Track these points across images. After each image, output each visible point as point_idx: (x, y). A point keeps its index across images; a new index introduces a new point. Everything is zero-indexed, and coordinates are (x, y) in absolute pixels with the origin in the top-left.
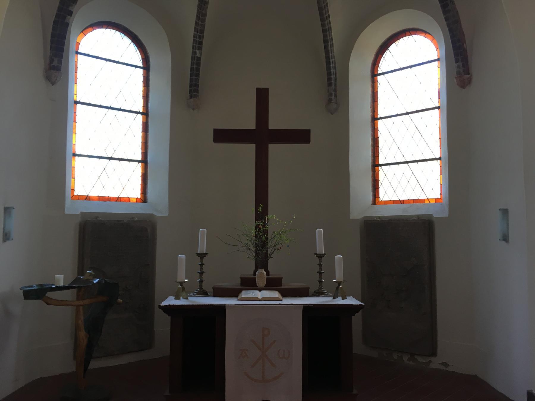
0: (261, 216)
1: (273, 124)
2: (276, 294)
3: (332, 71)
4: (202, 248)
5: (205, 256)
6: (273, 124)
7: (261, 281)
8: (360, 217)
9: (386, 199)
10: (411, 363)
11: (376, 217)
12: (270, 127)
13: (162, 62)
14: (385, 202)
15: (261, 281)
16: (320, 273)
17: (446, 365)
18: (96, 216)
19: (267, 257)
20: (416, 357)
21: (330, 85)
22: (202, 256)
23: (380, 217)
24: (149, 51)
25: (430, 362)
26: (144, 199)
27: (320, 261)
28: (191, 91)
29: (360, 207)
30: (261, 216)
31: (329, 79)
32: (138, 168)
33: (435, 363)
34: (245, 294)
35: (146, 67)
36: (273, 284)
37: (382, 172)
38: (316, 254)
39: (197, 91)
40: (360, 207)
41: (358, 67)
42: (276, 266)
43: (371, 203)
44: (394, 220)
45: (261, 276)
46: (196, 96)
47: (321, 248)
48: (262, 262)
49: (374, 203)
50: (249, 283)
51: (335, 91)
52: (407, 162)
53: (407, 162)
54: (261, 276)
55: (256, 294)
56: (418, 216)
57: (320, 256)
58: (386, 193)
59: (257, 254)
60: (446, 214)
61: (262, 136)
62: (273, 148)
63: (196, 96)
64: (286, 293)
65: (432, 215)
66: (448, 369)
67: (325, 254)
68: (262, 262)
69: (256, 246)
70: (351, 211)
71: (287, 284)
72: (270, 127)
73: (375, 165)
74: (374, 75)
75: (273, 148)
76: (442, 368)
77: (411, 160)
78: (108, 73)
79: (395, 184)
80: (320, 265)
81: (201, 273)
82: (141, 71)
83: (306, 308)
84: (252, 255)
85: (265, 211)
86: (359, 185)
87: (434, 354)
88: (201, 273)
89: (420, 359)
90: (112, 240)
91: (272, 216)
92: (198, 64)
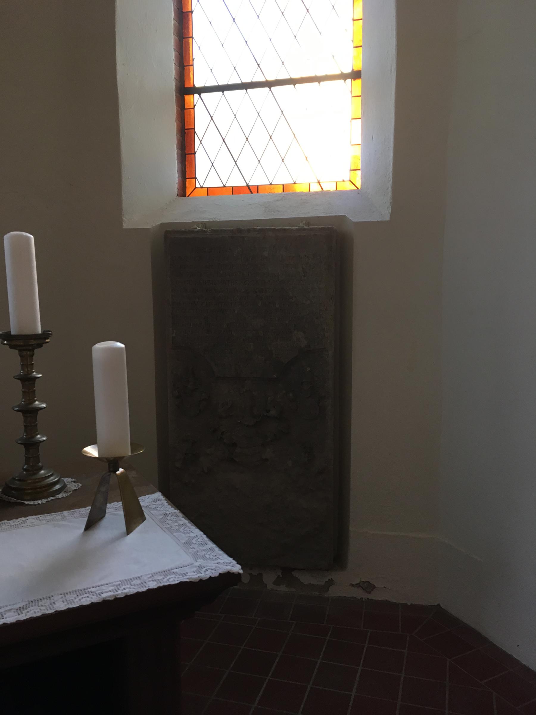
5: (40, 346)
9: (213, 182)
10: (283, 588)
11: (197, 223)
16: (29, 413)
17: (368, 587)
20: (295, 574)
23: (204, 224)
25: (331, 582)
27: (27, 363)
29: (147, 201)
33: (343, 585)
37: (202, 108)
38: (8, 336)
40: (147, 201)
43: (176, 191)
44: (249, 231)
47: (27, 313)
49: (183, 192)
52: (269, 84)
53: (269, 84)
56: (308, 221)
57: (27, 345)
58: (212, 169)
60: (383, 212)
65: (342, 219)
66: (376, 596)
67: (45, 335)
70: (125, 205)
73: (185, 90)
76: (359, 594)
77: (280, 77)
79: (235, 141)
80: (27, 381)
86: (145, 138)
87: (338, 559)
89: (306, 579)
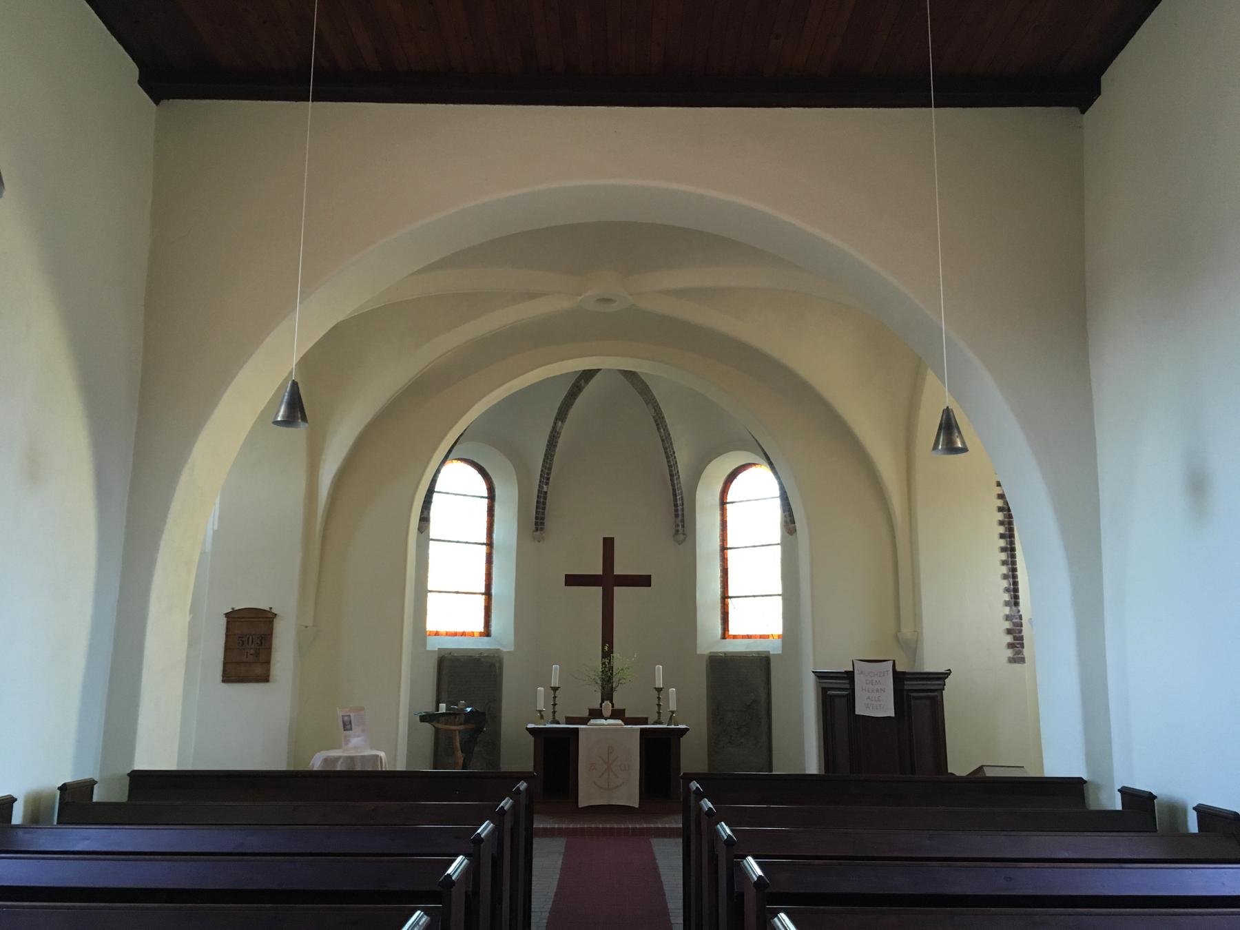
0: (607, 654)
1: (618, 570)
2: (620, 722)
3: (679, 502)
4: (555, 682)
6: (618, 570)
7: (607, 712)
8: (706, 652)
12: (616, 573)
13: (508, 495)
14: (735, 637)
15: (607, 712)
18: (450, 651)
19: (612, 690)
21: (677, 516)
22: (555, 689)
24: (495, 482)
26: (487, 633)
28: (536, 524)
30: (607, 654)
31: (676, 511)
32: (481, 600)
34: (592, 721)
35: (491, 497)
36: (617, 714)
39: (543, 524)
40: (709, 640)
41: (706, 497)
42: (619, 701)
45: (607, 708)
46: (542, 529)
47: (660, 684)
48: (607, 695)
50: (596, 713)
51: (683, 521)
54: (607, 708)
55: (603, 721)
56: (758, 653)
57: (659, 690)
59: (603, 688)
61: (608, 581)
62: (618, 591)
63: (542, 529)
64: (628, 721)
68: (607, 695)
69: (603, 680)
71: (627, 715)
72: (616, 573)
74: (723, 503)
75: (618, 591)
78: (461, 510)
81: (554, 705)
82: (486, 501)
83: (642, 730)
84: (599, 689)
85: (611, 650)
86: (708, 620)
88: (554, 705)
90: (466, 677)
91: (616, 654)
92: (545, 498)
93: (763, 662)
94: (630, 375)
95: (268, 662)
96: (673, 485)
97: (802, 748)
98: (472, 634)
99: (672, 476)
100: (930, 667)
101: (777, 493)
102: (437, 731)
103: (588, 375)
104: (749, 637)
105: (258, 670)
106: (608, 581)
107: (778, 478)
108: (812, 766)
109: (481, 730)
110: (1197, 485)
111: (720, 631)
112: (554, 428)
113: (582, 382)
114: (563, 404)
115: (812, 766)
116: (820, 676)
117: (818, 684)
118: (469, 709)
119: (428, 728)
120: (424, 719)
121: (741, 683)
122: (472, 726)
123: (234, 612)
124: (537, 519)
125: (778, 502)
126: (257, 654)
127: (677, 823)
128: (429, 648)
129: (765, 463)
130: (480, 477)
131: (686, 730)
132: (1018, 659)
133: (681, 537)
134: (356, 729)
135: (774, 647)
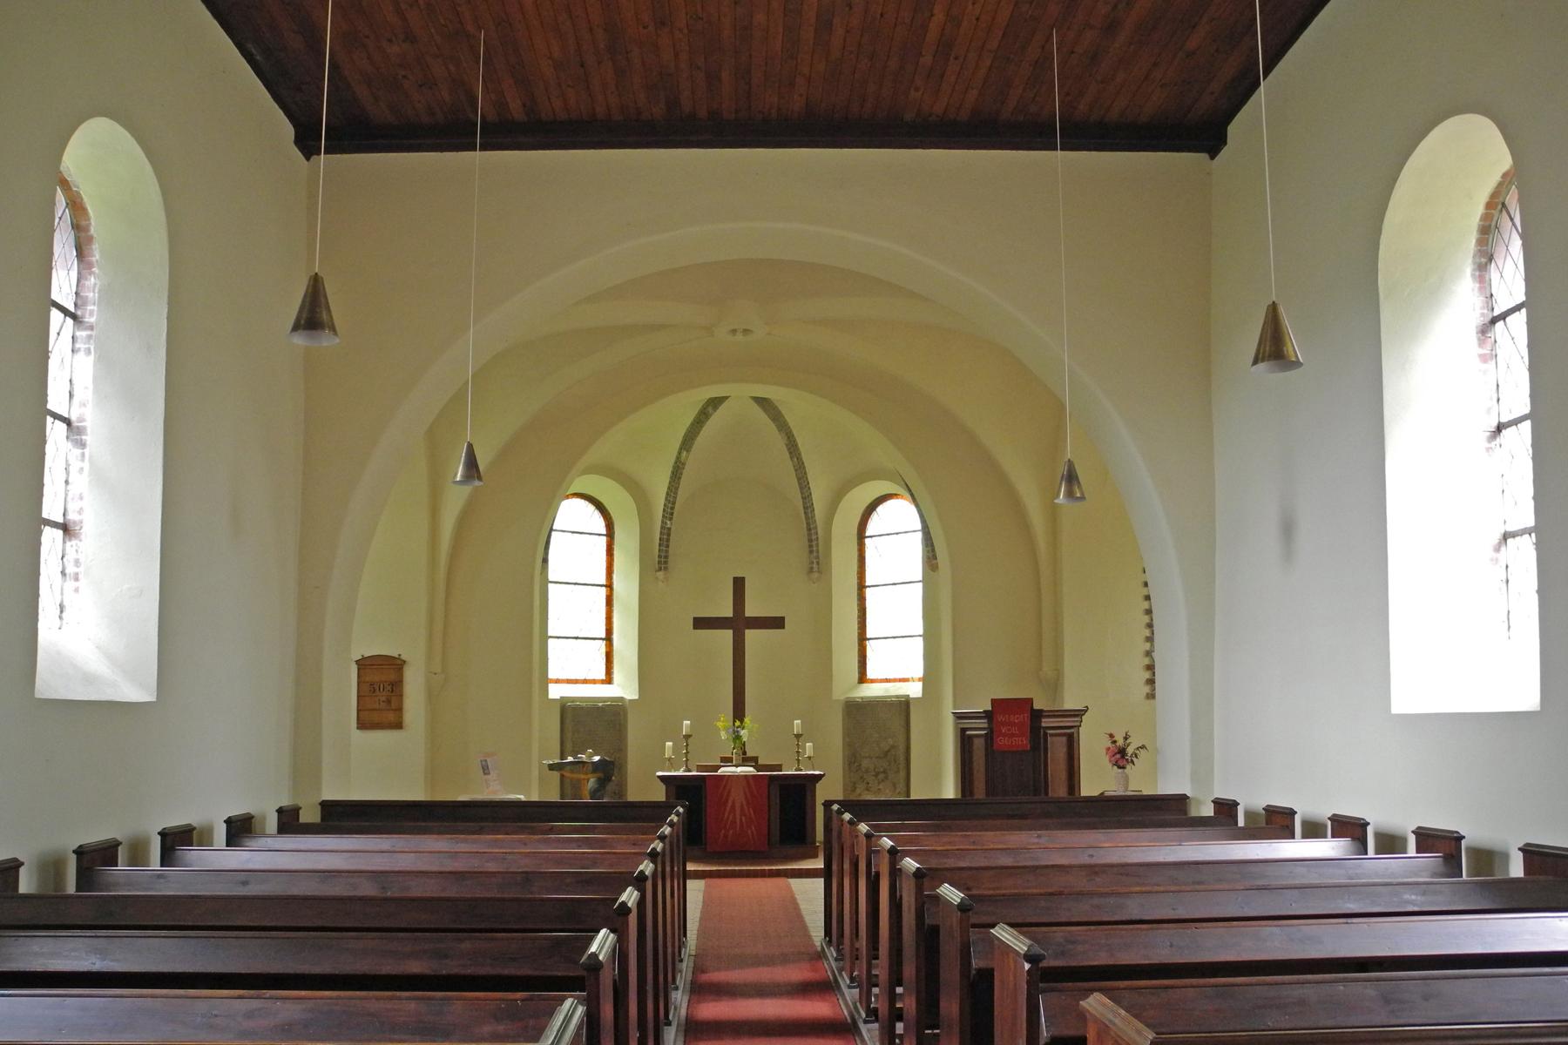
12: (747, 614)
14: (873, 681)
18: (573, 699)
35: (610, 534)
40: (845, 687)
50: (727, 761)
61: (739, 623)
72: (747, 614)
82: (604, 539)
93: (904, 705)
94: (761, 402)
95: (400, 709)
96: (807, 518)
97: (939, 778)
98: (594, 682)
99: (805, 508)
100: (1070, 704)
101: (917, 524)
102: (562, 776)
103: (715, 403)
104: (887, 681)
105: (391, 717)
106: (739, 623)
107: (917, 506)
108: (949, 791)
109: (609, 779)
110: (1288, 530)
111: (856, 676)
112: (678, 458)
113: (710, 409)
114: (686, 435)
115: (949, 791)
116: (959, 717)
117: (956, 724)
118: (597, 758)
119: (556, 775)
120: (552, 767)
121: (879, 727)
122: (600, 775)
123: (364, 658)
124: (659, 558)
125: (919, 535)
126: (389, 702)
127: (819, 864)
128: (551, 696)
129: (907, 495)
130: (597, 514)
131: (820, 777)
132: (1151, 696)
133: (816, 575)
134: (493, 775)
135: (915, 690)
